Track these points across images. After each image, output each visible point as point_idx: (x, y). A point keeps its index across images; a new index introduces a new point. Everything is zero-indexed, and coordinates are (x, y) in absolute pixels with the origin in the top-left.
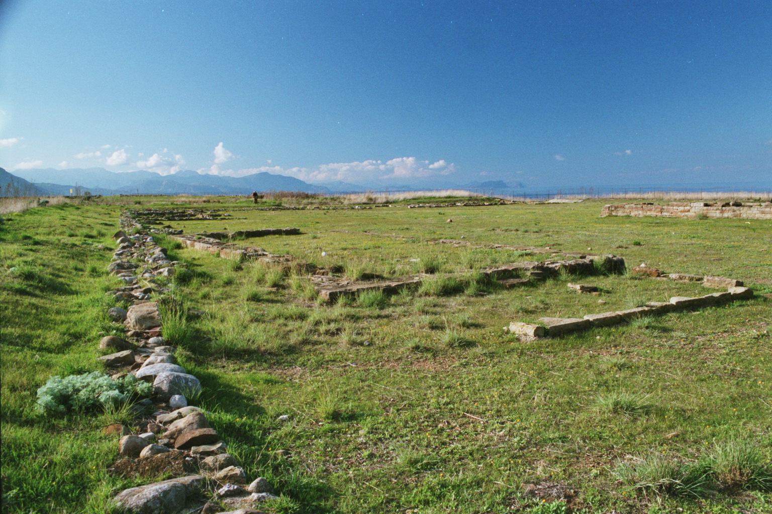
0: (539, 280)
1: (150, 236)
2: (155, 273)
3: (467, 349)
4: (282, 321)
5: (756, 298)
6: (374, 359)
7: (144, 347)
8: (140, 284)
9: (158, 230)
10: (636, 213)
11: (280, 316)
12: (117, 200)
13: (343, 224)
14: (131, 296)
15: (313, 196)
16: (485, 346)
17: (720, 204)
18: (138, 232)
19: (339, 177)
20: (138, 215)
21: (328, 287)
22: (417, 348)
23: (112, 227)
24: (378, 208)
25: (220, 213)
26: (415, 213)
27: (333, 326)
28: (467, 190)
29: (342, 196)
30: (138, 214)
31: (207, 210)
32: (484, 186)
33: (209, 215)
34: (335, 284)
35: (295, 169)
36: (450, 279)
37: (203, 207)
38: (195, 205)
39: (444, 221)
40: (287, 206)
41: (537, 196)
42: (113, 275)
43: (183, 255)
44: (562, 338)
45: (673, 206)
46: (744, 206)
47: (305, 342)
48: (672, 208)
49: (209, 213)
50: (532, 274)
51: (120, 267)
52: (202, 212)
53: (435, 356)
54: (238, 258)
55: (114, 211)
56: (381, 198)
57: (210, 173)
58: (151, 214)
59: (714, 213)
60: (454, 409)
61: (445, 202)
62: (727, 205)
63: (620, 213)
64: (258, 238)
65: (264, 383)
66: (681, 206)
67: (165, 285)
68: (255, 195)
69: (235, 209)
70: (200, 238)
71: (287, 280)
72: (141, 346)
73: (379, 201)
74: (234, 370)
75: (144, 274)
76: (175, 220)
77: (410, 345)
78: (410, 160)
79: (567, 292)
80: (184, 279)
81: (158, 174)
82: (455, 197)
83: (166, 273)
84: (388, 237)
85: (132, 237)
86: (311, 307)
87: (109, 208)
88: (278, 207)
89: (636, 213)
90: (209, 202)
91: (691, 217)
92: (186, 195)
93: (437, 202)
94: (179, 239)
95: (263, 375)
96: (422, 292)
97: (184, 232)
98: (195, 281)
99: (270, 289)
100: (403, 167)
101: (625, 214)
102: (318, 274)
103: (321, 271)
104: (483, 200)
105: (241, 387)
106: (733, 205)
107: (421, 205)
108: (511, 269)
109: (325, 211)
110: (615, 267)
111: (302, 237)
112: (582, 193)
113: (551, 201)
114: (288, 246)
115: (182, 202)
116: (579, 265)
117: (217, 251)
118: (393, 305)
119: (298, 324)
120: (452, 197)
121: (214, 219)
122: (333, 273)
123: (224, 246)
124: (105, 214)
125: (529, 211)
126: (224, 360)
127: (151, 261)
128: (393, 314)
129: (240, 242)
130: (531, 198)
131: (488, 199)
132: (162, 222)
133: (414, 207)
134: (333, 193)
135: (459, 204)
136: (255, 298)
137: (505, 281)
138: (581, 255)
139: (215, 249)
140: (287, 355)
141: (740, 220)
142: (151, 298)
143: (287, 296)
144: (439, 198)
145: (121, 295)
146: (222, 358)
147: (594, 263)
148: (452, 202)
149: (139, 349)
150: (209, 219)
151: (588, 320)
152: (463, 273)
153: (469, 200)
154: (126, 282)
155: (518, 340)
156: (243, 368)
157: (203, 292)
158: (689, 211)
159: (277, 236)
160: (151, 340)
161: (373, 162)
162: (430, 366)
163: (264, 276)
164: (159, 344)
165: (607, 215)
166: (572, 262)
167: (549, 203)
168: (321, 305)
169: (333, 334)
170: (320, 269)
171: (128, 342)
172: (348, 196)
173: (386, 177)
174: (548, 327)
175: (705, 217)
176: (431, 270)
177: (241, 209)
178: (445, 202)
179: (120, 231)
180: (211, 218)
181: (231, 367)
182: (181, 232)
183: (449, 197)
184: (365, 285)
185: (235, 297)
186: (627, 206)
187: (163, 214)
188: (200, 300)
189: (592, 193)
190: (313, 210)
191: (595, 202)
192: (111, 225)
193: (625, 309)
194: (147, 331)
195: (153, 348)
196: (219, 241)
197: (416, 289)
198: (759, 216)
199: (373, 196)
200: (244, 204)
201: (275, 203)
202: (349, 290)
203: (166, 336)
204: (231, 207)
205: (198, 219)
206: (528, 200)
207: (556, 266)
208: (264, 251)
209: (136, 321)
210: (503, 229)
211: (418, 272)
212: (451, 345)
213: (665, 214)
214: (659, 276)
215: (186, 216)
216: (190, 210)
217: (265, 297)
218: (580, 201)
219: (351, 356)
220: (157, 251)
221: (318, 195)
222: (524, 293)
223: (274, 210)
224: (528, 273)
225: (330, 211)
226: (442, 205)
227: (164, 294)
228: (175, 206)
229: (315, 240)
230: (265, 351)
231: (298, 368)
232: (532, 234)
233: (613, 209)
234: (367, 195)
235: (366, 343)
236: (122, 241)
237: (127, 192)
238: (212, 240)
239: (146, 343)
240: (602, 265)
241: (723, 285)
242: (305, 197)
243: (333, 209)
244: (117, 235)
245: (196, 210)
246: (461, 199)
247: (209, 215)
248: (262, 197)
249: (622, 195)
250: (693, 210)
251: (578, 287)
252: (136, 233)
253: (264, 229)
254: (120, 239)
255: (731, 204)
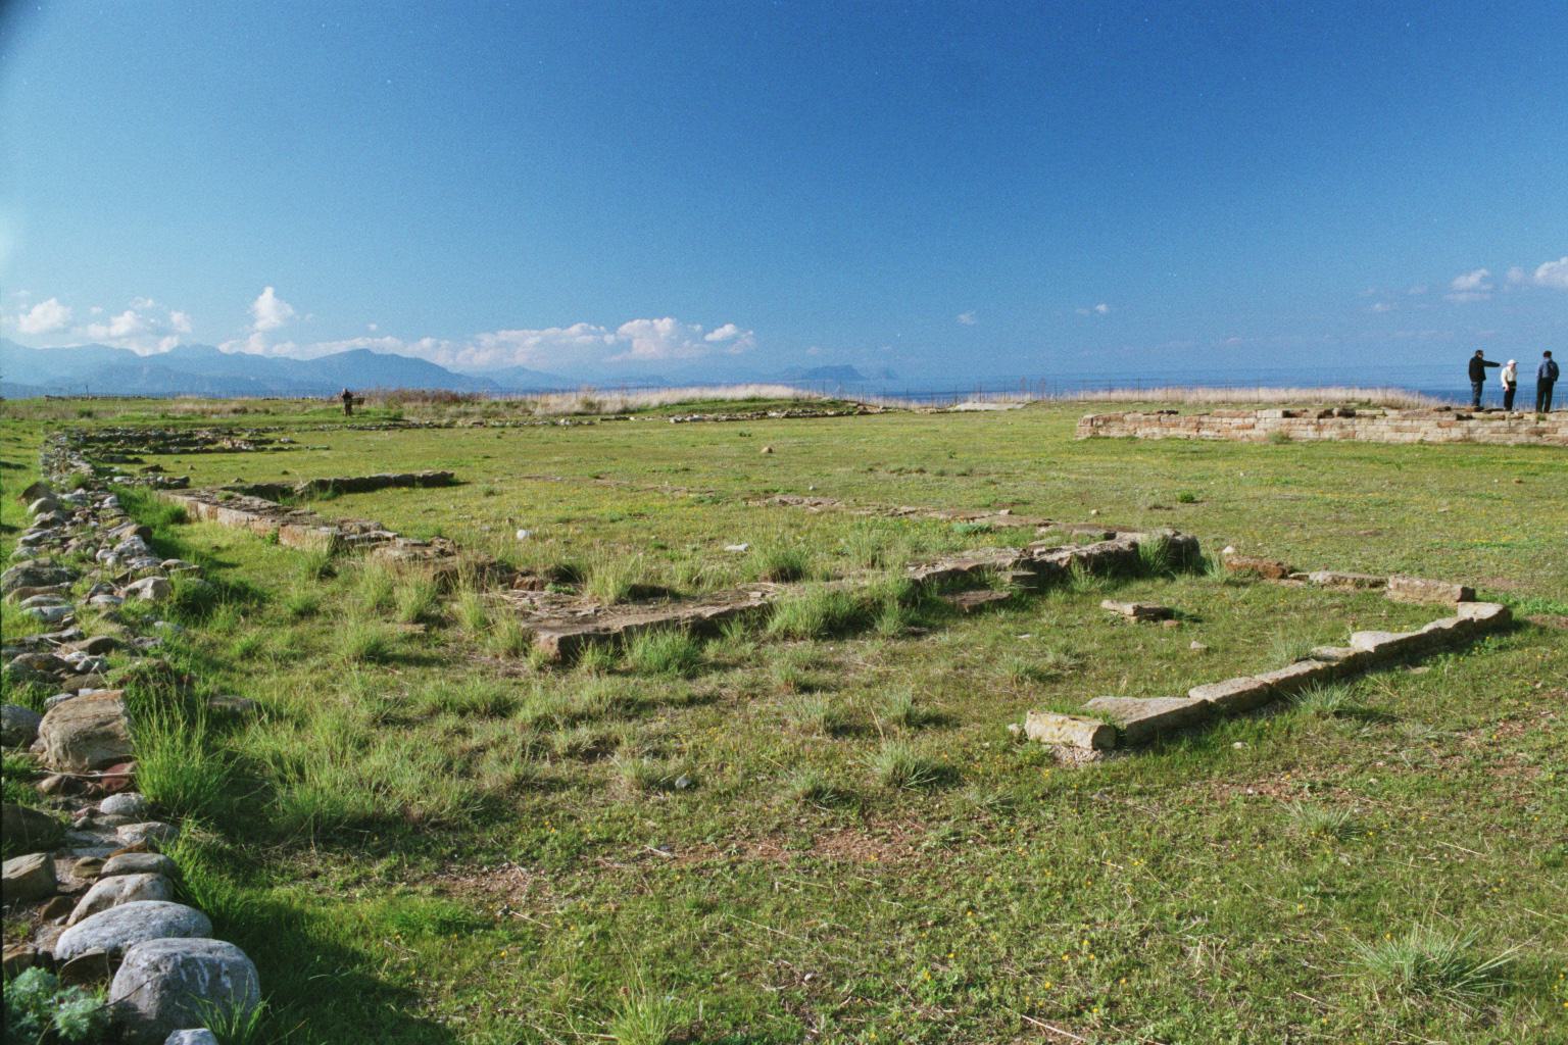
0: (1031, 593)
1: (110, 492)
2: (121, 592)
3: (941, 792)
4: (451, 721)
5: (1519, 626)
6: (713, 830)
7: (88, 826)
8: (84, 625)
9: (131, 475)
10: (1148, 431)
11: (445, 705)
12: (39, 408)
13: (544, 460)
14: (55, 664)
15: (469, 399)
16: (986, 782)
17: (1313, 412)
18: (84, 484)
19: (520, 359)
20: (83, 442)
21: (552, 623)
22: (816, 794)
23: (20, 473)
24: (606, 423)
25: (270, 436)
26: (689, 433)
27: (584, 734)
28: (788, 385)
29: (529, 398)
30: (84, 438)
31: (242, 430)
32: (814, 376)
33: (246, 441)
34: (565, 612)
35: (427, 342)
36: (836, 595)
37: (233, 424)
38: (215, 419)
39: (754, 451)
40: (414, 420)
41: (931, 396)
42: (11, 602)
43: (191, 540)
44: (1161, 752)
45: (1220, 416)
46: (1360, 416)
47: (523, 784)
48: (1218, 420)
49: (246, 436)
50: (1015, 578)
51: (32, 579)
52: (231, 433)
53: (865, 814)
54: (325, 548)
55: (31, 433)
56: (613, 401)
57: (247, 351)
58: (117, 439)
59: (1303, 430)
60: (989, 1004)
61: (745, 409)
62: (1328, 414)
63: (1115, 432)
64: (360, 495)
65: (439, 933)
66: (1238, 416)
67: (148, 624)
68: (347, 396)
69: (304, 427)
70: (229, 498)
71: (447, 604)
72: (77, 824)
73: (609, 408)
74: (345, 886)
75: (92, 595)
76: (170, 452)
77: (800, 783)
78: (665, 325)
79: (1105, 620)
80: (195, 608)
81: (133, 353)
82: (766, 400)
83: (148, 593)
84: (655, 490)
85: (66, 497)
86: (516, 675)
87: (20, 425)
88: (396, 423)
89: (1148, 431)
90: (244, 411)
91: (1258, 437)
92: (196, 397)
93: (728, 410)
94: (181, 501)
95: (423, 902)
96: (778, 630)
97: (192, 481)
98: (223, 614)
99: (410, 628)
100: (650, 338)
101: (1125, 434)
102: (518, 587)
103: (527, 579)
104: (823, 405)
105: (374, 949)
106: (1340, 414)
107: (696, 416)
108: (966, 567)
109: (497, 431)
110: (1182, 557)
111: (461, 491)
112: (1024, 390)
113: (962, 407)
114: (433, 514)
115: (187, 411)
116: (1108, 554)
117: (271, 531)
118: (716, 666)
119: (494, 729)
120: (760, 400)
121: (258, 450)
122: (555, 583)
123: (287, 516)
124: (9, 440)
125: (923, 428)
126: (314, 851)
127: (110, 561)
128: (724, 691)
129: (322, 504)
130: (919, 400)
131: (834, 404)
132: (140, 457)
133: (682, 421)
134: (509, 392)
135: (774, 414)
136: (376, 655)
137: (958, 598)
138: (1104, 532)
139: (266, 525)
140: (484, 826)
141: (1355, 445)
142: (109, 668)
143: (451, 644)
144: (733, 401)
145: (28, 662)
146: (308, 846)
147: (1141, 550)
148: (759, 409)
149: (71, 834)
150: (247, 451)
151: (1205, 702)
152: (861, 583)
153: (794, 406)
154: (46, 621)
155: (1054, 759)
156: (368, 877)
157: (244, 640)
158: (1253, 427)
159: (405, 489)
160: (107, 804)
161: (589, 324)
162: (862, 848)
163: (390, 592)
164: (130, 816)
165: (1089, 435)
166: (1093, 548)
167: (957, 412)
168: (540, 669)
169: (590, 756)
170: (524, 575)
171: (38, 816)
172: (544, 400)
173: (616, 358)
174: (1123, 725)
175: (1284, 439)
176: (789, 573)
177: (315, 427)
178: (745, 409)
179: (37, 485)
180: (251, 448)
181: (337, 874)
182: (183, 484)
183: (753, 400)
184: (637, 616)
185: (326, 650)
186: (1128, 418)
187: (143, 440)
188: (237, 664)
189: (1044, 389)
190: (471, 427)
191: (1050, 408)
192: (18, 467)
193: (1261, 669)
194: (98, 774)
195: (111, 828)
196: (275, 504)
197: (762, 623)
198: (1390, 436)
199: (596, 398)
200: (321, 417)
201: (388, 413)
202: (607, 629)
203: (149, 791)
204: (294, 423)
205: (223, 450)
206: (914, 405)
207: (1061, 559)
208: (383, 529)
209: (64, 748)
210: (892, 469)
211: (755, 578)
212: (897, 780)
213: (1203, 433)
214: (1284, 576)
215: (195, 443)
216: (204, 429)
217: (402, 650)
218: (1019, 406)
219: (650, 823)
220: (128, 534)
221: (479, 396)
222: (1011, 627)
223: (387, 428)
224: (1007, 577)
225: (507, 431)
226: (739, 415)
227: (145, 653)
228: (172, 422)
229: (493, 500)
230: (424, 819)
231: (519, 870)
232: (957, 479)
233: (1100, 423)
234: (581, 396)
235: (680, 782)
236: (42, 508)
237: (61, 389)
238: (257, 502)
239: (93, 814)
240: (1158, 554)
241: (1433, 596)
242: (450, 401)
243: (514, 426)
244: (30, 493)
245: (217, 431)
246: (777, 404)
247: (246, 441)
248: (360, 401)
249: (1102, 395)
250: (1261, 425)
251: (1128, 609)
252: (78, 487)
253: (374, 475)
254: (38, 501)
255: (1335, 412)
